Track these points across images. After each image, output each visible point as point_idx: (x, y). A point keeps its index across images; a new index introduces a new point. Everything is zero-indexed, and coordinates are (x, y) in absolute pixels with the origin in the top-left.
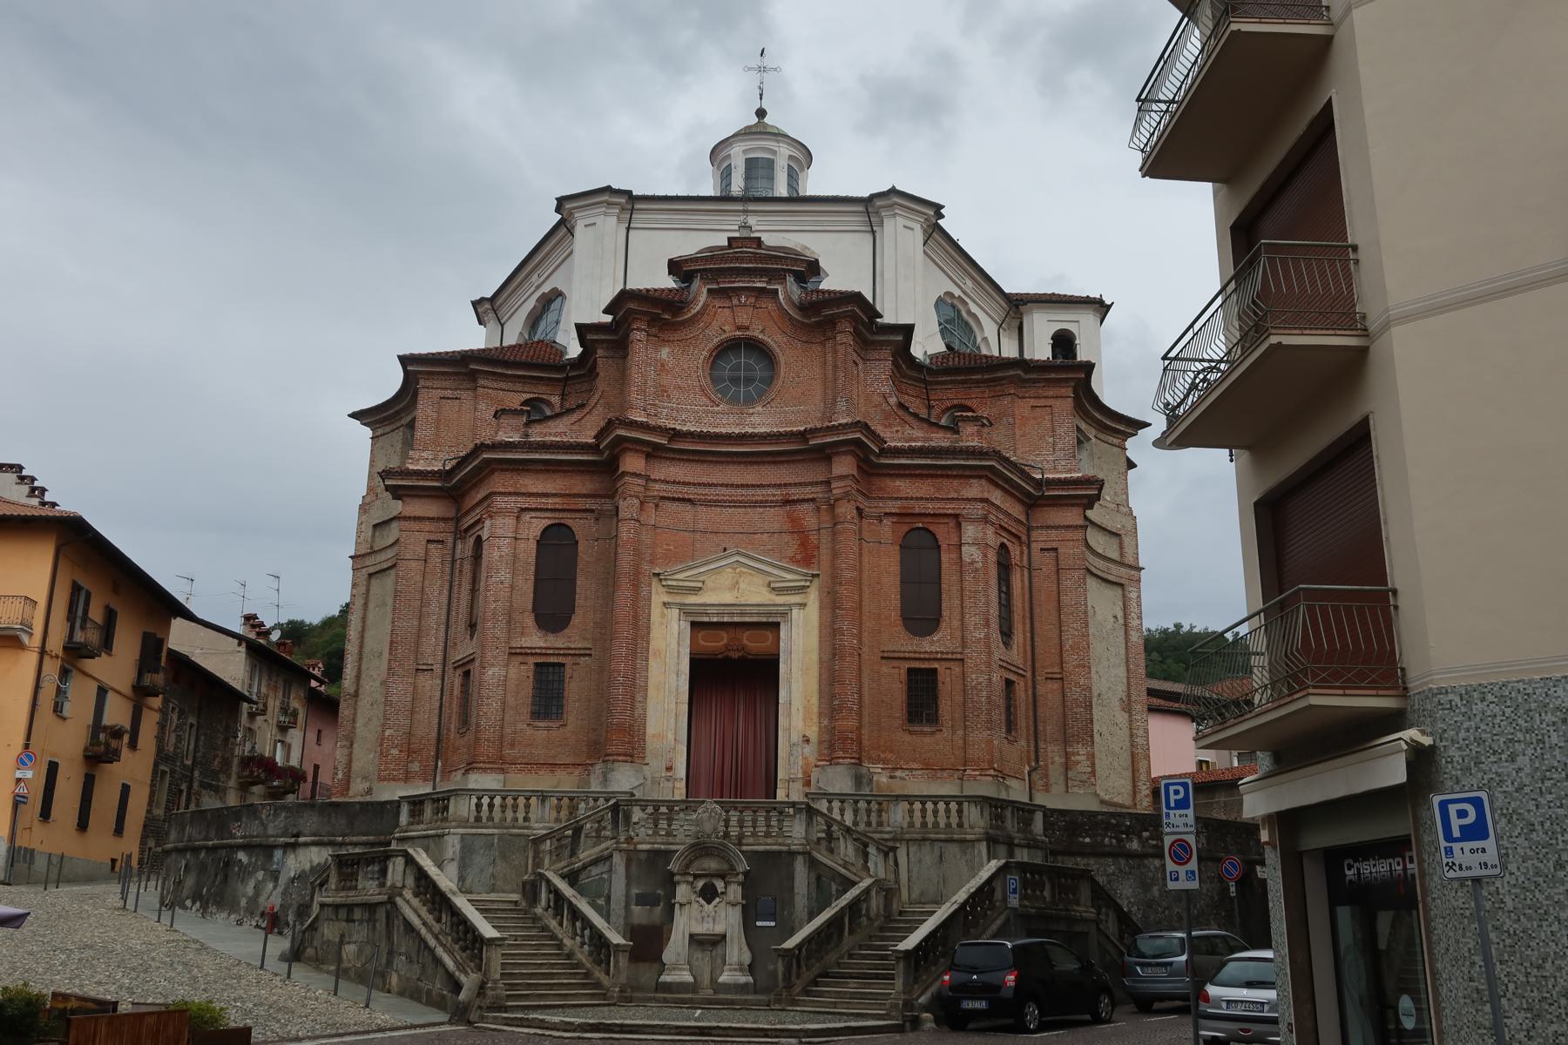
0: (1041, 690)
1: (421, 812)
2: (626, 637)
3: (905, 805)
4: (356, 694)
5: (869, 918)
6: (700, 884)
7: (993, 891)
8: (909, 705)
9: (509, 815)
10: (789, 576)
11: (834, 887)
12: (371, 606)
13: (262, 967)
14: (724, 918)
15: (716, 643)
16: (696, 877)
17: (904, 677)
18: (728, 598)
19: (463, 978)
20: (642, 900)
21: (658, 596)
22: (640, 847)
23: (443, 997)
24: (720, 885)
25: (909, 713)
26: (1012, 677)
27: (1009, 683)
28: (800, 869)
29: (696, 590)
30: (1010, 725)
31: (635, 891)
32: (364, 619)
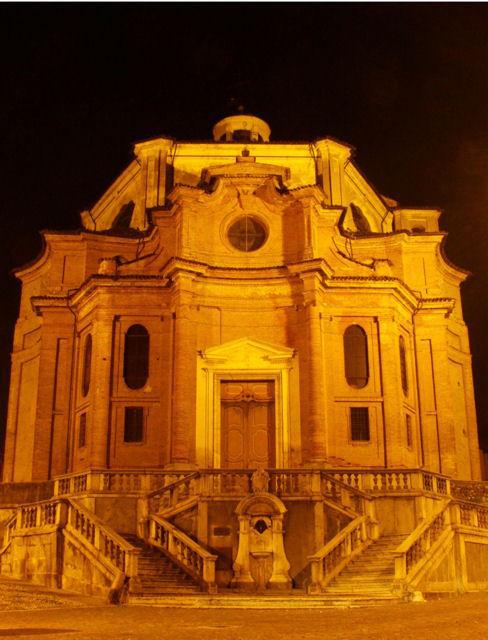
0: (424, 422)
1: (68, 487)
2: (178, 390)
3: (372, 477)
4: (16, 434)
5: (362, 541)
6: (256, 520)
7: (443, 520)
8: (353, 429)
9: (125, 485)
10: (279, 353)
11: (338, 523)
12: (23, 381)
13: (59, 340)
14: (274, 543)
15: (235, 391)
16: (252, 516)
17: (348, 412)
18: (242, 366)
19: (112, 578)
20: (218, 532)
21: (200, 363)
22: (216, 499)
23: (98, 589)
24: (267, 521)
25: (353, 433)
26: (409, 413)
27: (408, 416)
28: (319, 510)
29: (222, 362)
30: (409, 443)
31: (213, 527)
32: (19, 389)
